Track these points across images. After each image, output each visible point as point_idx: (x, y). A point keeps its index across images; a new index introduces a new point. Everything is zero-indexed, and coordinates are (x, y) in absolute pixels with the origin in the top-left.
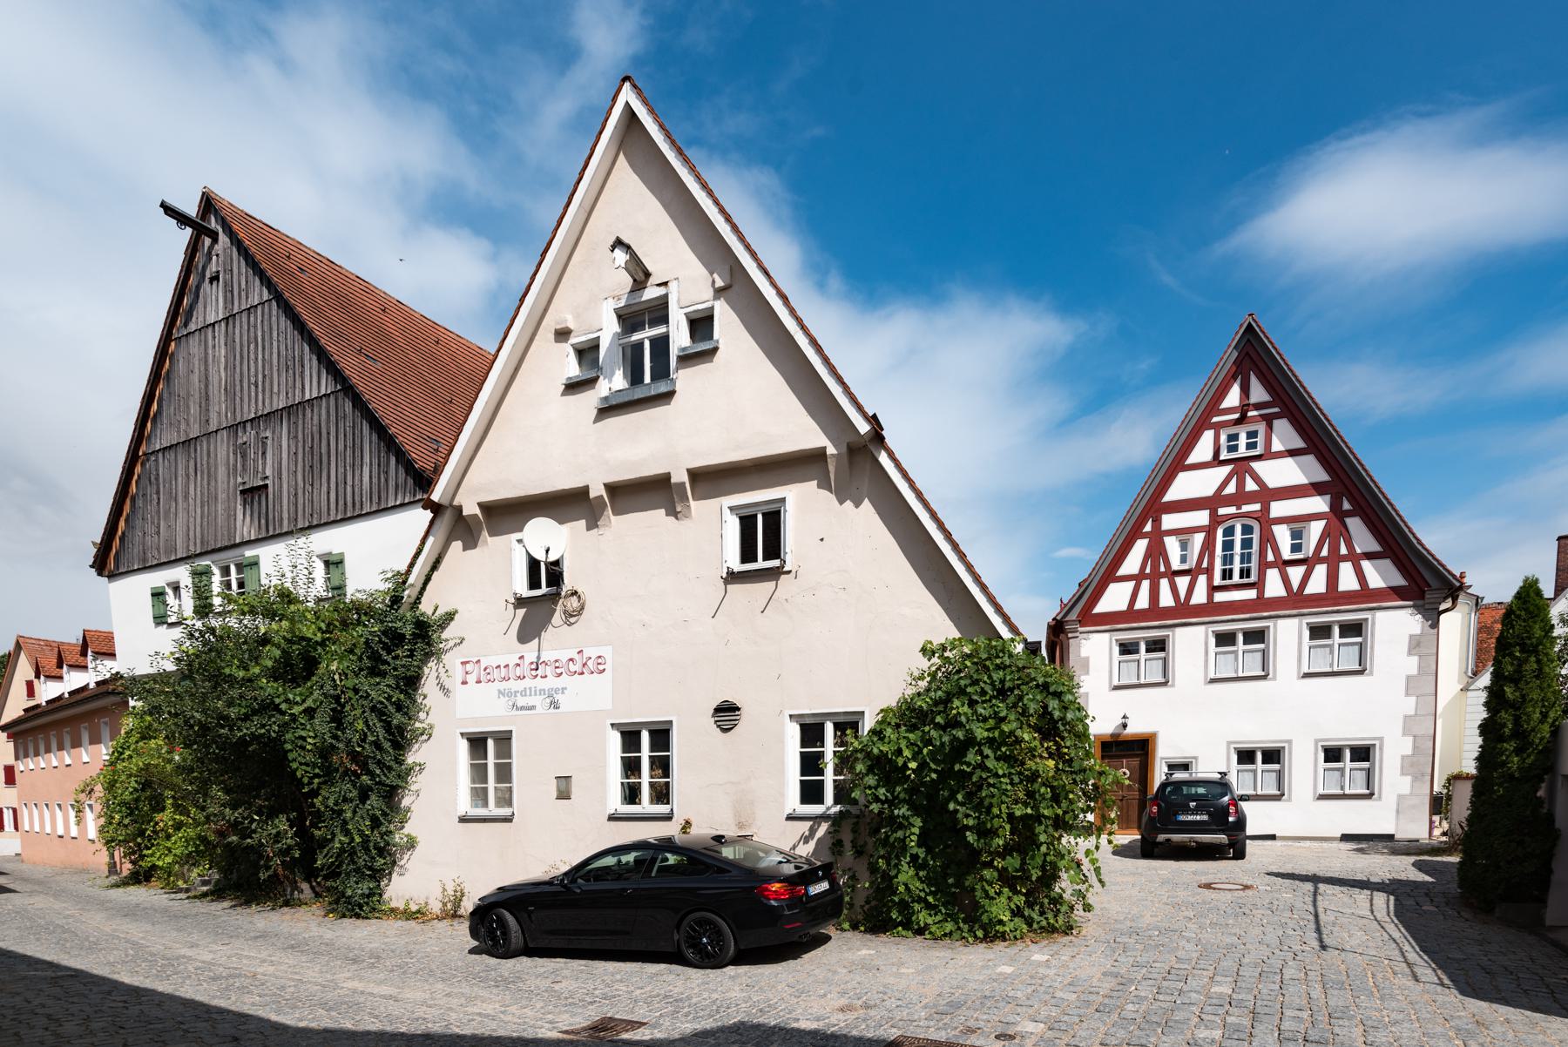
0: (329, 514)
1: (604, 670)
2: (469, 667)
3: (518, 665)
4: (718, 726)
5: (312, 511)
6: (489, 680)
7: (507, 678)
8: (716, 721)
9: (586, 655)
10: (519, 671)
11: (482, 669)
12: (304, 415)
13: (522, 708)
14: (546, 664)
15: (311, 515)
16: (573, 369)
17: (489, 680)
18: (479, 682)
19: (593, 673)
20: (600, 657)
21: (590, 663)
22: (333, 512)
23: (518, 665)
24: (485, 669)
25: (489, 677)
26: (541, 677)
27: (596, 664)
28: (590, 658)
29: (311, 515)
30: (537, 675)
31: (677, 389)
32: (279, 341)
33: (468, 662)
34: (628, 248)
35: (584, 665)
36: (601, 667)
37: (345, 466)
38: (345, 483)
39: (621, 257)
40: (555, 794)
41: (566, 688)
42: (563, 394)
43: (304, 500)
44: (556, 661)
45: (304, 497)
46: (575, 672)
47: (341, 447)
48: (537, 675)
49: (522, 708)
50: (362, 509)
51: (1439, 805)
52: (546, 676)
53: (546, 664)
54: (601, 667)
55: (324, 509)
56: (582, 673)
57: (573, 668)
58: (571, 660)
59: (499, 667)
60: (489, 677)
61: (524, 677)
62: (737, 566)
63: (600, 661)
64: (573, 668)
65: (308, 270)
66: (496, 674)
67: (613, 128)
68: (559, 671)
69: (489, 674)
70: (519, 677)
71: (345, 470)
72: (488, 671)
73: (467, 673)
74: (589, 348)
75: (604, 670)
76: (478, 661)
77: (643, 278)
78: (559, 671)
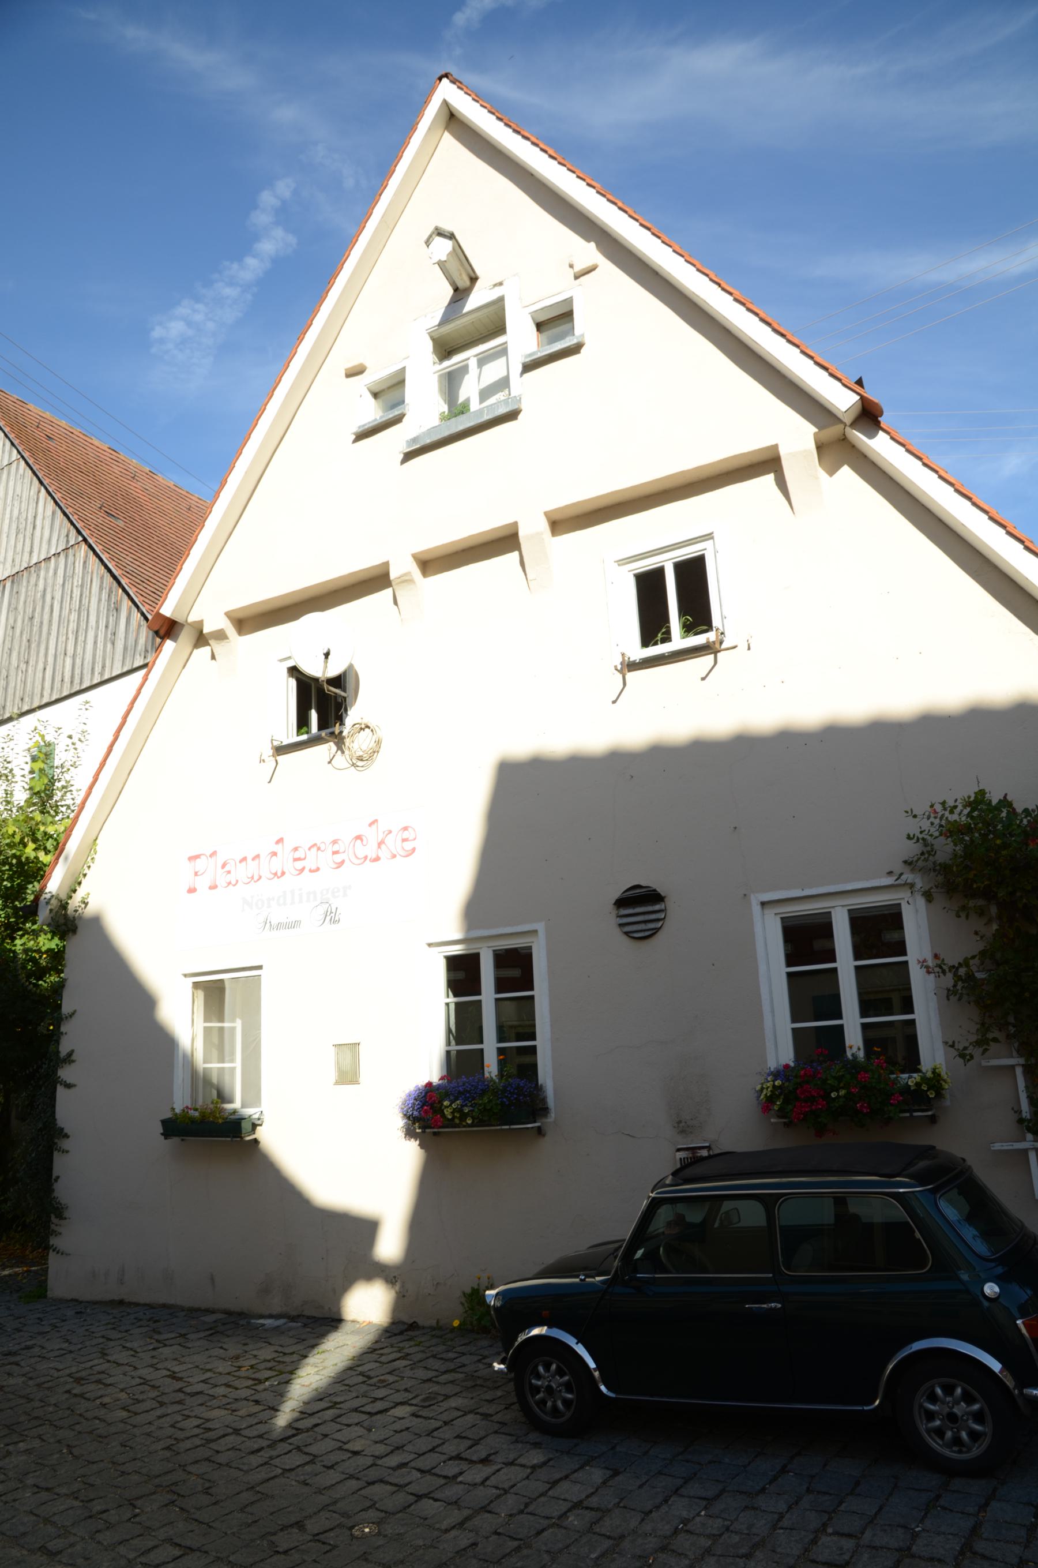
0: (42, 696)
1: (414, 850)
2: (200, 864)
3: (274, 854)
4: (626, 933)
5: (24, 693)
6: (230, 883)
7: (256, 878)
8: (621, 925)
9: (383, 826)
10: (276, 865)
11: (220, 865)
12: (28, 582)
13: (279, 926)
14: (319, 849)
15: (22, 699)
16: (372, 412)
17: (230, 883)
18: (213, 887)
19: (394, 856)
20: (405, 829)
21: (389, 840)
22: (46, 693)
23: (274, 854)
24: (224, 866)
25: (229, 878)
26: (311, 871)
27: (399, 842)
28: (390, 832)
29: (22, 699)
30: (304, 868)
31: (523, 407)
32: (13, 505)
33: (197, 857)
34: (451, 236)
35: (380, 845)
36: (408, 846)
37: (67, 634)
38: (65, 654)
39: (443, 248)
40: (332, 1075)
41: (909, 835)
42: (403, 370)
43: (16, 684)
44: (335, 842)
45: (16, 678)
46: (366, 858)
47: (66, 612)
48: (304, 868)
49: (279, 926)
50: (81, 683)
51: (76, 911)
52: (318, 869)
53: (319, 849)
54: (408, 846)
55: (37, 691)
56: (377, 859)
57: (361, 850)
58: (359, 837)
59: (244, 859)
60: (229, 878)
61: (283, 873)
62: (640, 653)
63: (406, 835)
64: (361, 850)
65: (56, 439)
66: (241, 872)
67: (420, 126)
68: (338, 858)
69: (229, 872)
70: (276, 874)
71: (67, 639)
72: (227, 868)
73: (196, 874)
74: (389, 388)
75: (414, 850)
76: (214, 854)
77: (468, 283)
78: (338, 858)
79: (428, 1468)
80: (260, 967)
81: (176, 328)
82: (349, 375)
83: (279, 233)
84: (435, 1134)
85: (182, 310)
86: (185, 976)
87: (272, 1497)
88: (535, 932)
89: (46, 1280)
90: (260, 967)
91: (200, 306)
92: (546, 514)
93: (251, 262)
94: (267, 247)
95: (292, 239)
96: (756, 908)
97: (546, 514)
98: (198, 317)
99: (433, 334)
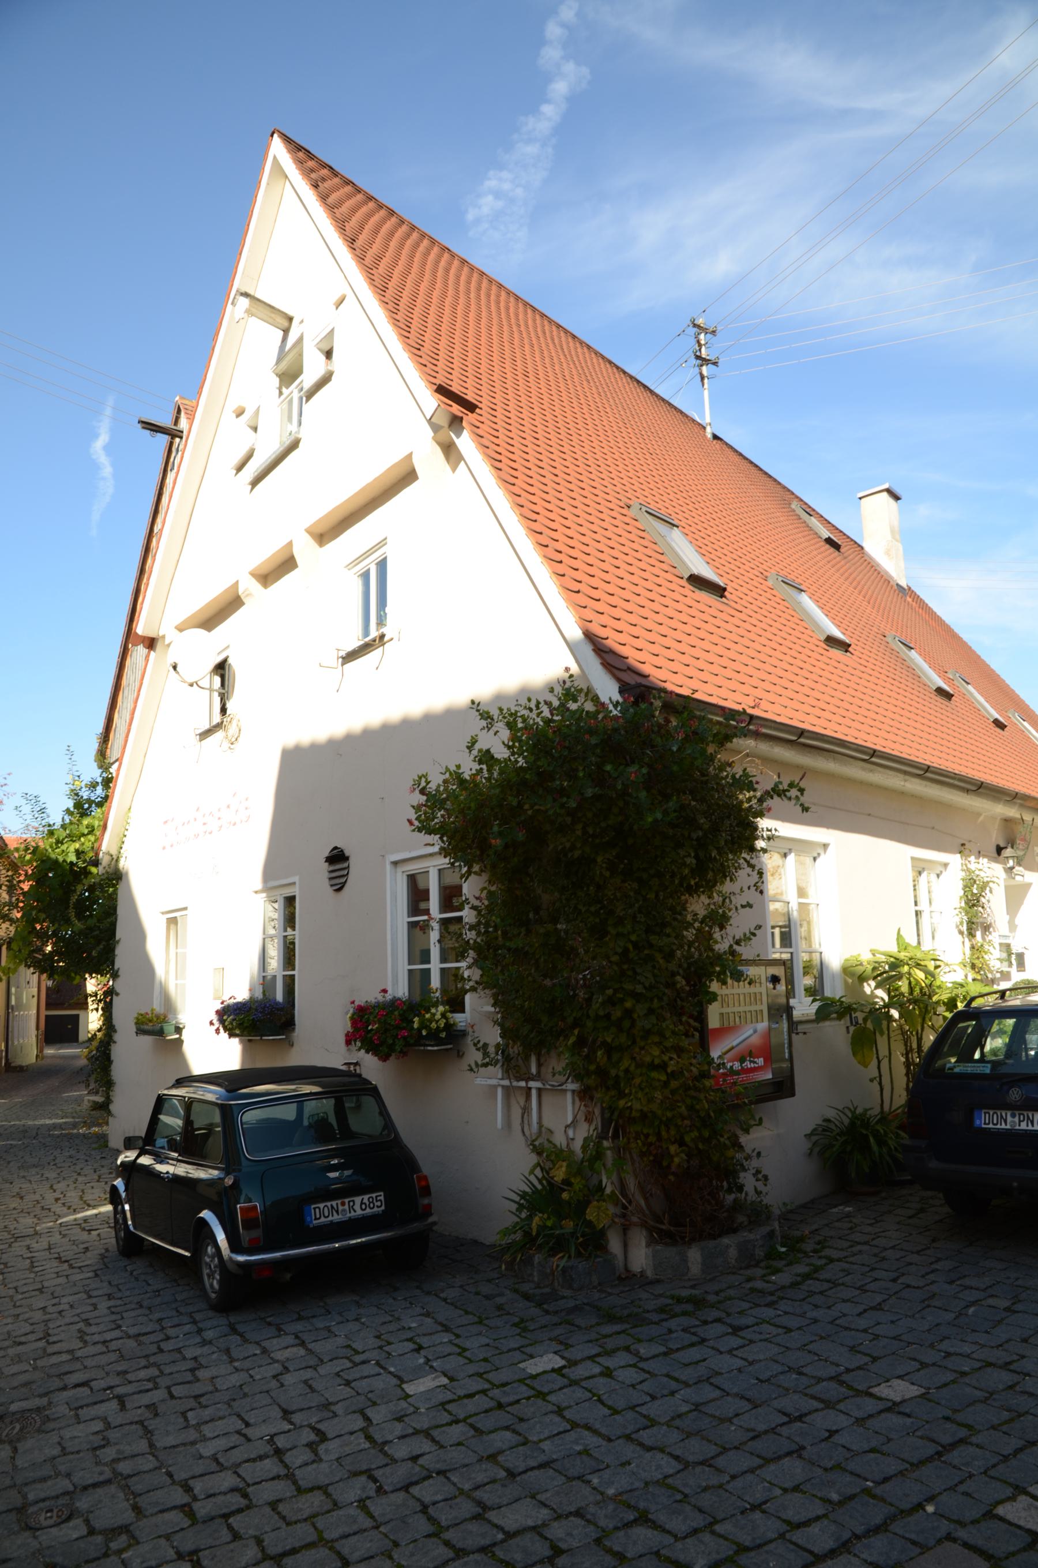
79: (989, 1370)
80: (185, 909)
81: (488, 204)
82: (238, 416)
83: (570, 67)
84: (250, 1041)
85: (491, 183)
86: (163, 913)
87: (550, 1339)
88: (294, 883)
89: (397, 1135)
90: (185, 909)
91: (505, 174)
92: (309, 531)
93: (547, 109)
94: (560, 88)
95: (585, 71)
96: (388, 867)
97: (309, 531)
98: (506, 186)
99: (277, 371)
